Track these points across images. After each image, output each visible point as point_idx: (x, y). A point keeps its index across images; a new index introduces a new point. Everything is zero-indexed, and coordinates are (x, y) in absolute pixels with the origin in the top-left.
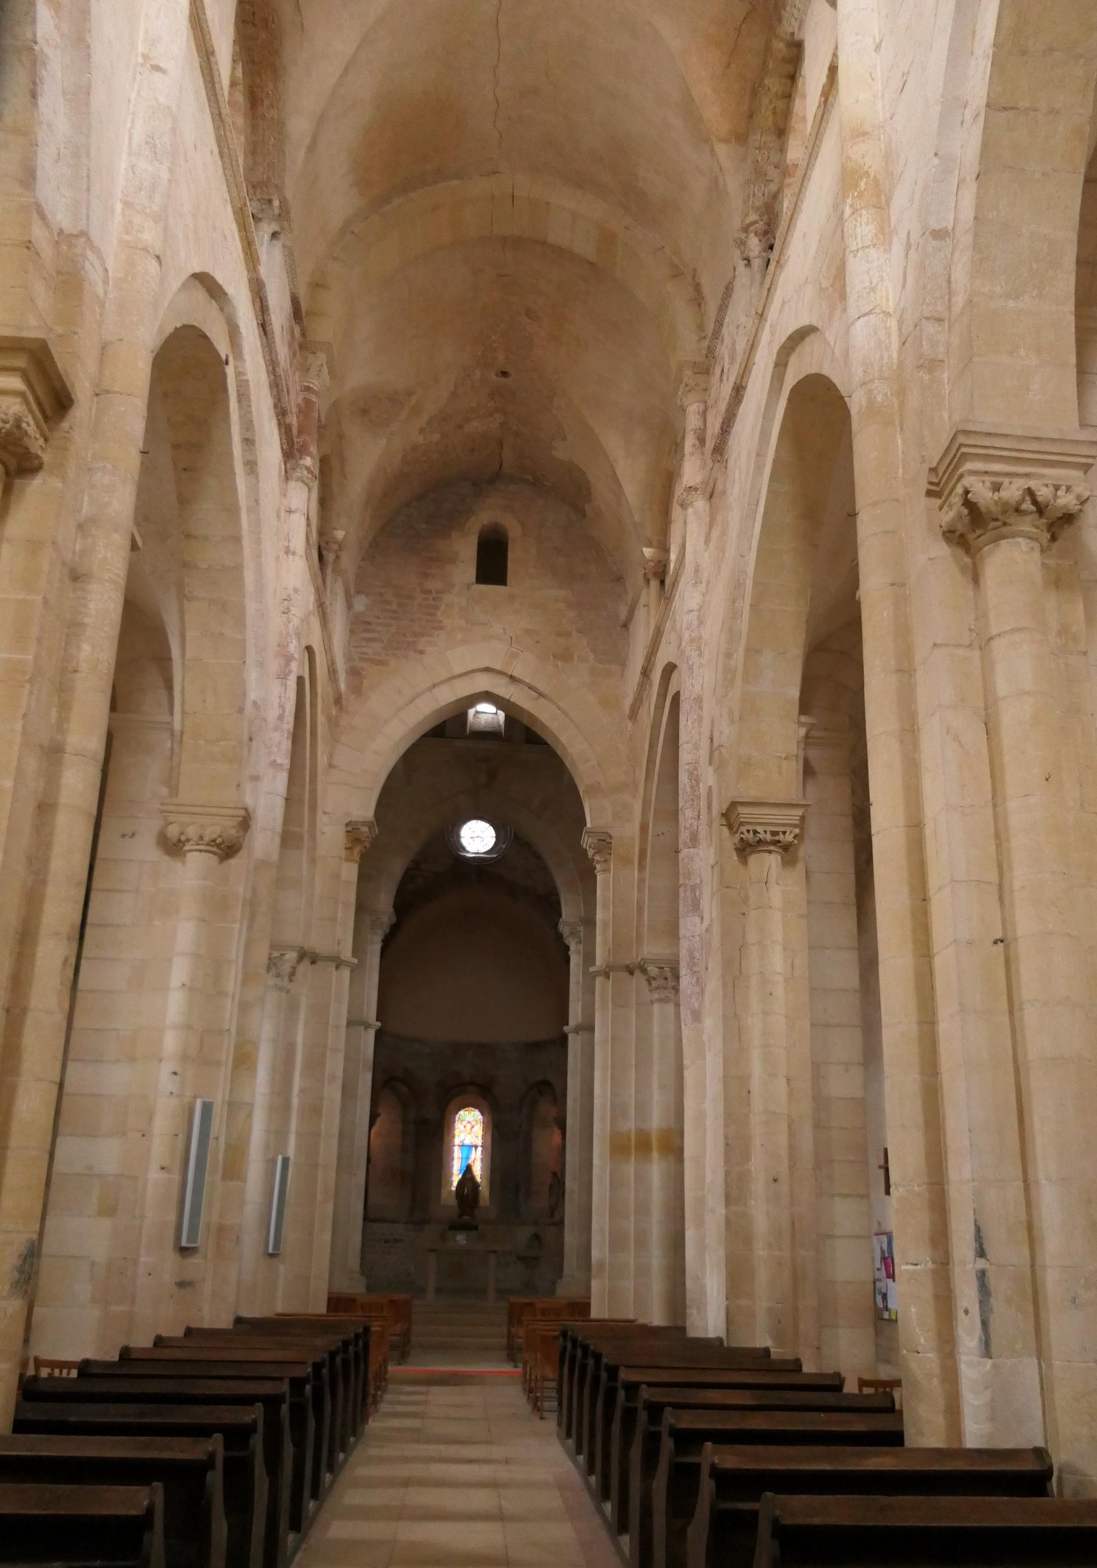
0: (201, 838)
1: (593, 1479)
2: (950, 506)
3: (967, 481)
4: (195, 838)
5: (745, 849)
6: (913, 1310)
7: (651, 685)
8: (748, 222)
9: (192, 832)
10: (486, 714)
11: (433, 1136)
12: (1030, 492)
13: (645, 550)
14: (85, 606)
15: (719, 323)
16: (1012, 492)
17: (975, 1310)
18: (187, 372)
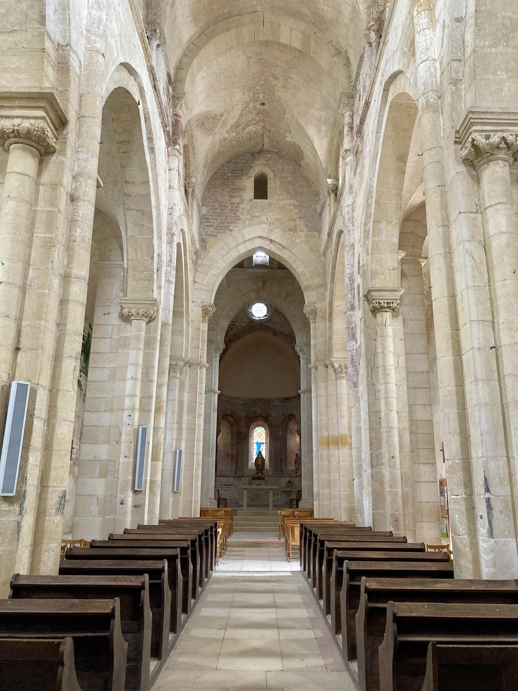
0: (138, 314)
1: (315, 589)
2: (466, 148)
3: (474, 135)
4: (135, 314)
5: (375, 311)
6: (457, 516)
7: (332, 240)
8: (370, 25)
9: (133, 311)
10: (260, 257)
11: (242, 439)
12: (504, 139)
13: (328, 180)
14: (77, 212)
15: (358, 74)
16: (495, 139)
17: (485, 516)
18: (121, 108)
